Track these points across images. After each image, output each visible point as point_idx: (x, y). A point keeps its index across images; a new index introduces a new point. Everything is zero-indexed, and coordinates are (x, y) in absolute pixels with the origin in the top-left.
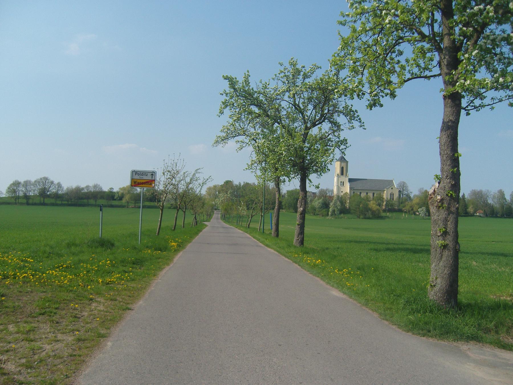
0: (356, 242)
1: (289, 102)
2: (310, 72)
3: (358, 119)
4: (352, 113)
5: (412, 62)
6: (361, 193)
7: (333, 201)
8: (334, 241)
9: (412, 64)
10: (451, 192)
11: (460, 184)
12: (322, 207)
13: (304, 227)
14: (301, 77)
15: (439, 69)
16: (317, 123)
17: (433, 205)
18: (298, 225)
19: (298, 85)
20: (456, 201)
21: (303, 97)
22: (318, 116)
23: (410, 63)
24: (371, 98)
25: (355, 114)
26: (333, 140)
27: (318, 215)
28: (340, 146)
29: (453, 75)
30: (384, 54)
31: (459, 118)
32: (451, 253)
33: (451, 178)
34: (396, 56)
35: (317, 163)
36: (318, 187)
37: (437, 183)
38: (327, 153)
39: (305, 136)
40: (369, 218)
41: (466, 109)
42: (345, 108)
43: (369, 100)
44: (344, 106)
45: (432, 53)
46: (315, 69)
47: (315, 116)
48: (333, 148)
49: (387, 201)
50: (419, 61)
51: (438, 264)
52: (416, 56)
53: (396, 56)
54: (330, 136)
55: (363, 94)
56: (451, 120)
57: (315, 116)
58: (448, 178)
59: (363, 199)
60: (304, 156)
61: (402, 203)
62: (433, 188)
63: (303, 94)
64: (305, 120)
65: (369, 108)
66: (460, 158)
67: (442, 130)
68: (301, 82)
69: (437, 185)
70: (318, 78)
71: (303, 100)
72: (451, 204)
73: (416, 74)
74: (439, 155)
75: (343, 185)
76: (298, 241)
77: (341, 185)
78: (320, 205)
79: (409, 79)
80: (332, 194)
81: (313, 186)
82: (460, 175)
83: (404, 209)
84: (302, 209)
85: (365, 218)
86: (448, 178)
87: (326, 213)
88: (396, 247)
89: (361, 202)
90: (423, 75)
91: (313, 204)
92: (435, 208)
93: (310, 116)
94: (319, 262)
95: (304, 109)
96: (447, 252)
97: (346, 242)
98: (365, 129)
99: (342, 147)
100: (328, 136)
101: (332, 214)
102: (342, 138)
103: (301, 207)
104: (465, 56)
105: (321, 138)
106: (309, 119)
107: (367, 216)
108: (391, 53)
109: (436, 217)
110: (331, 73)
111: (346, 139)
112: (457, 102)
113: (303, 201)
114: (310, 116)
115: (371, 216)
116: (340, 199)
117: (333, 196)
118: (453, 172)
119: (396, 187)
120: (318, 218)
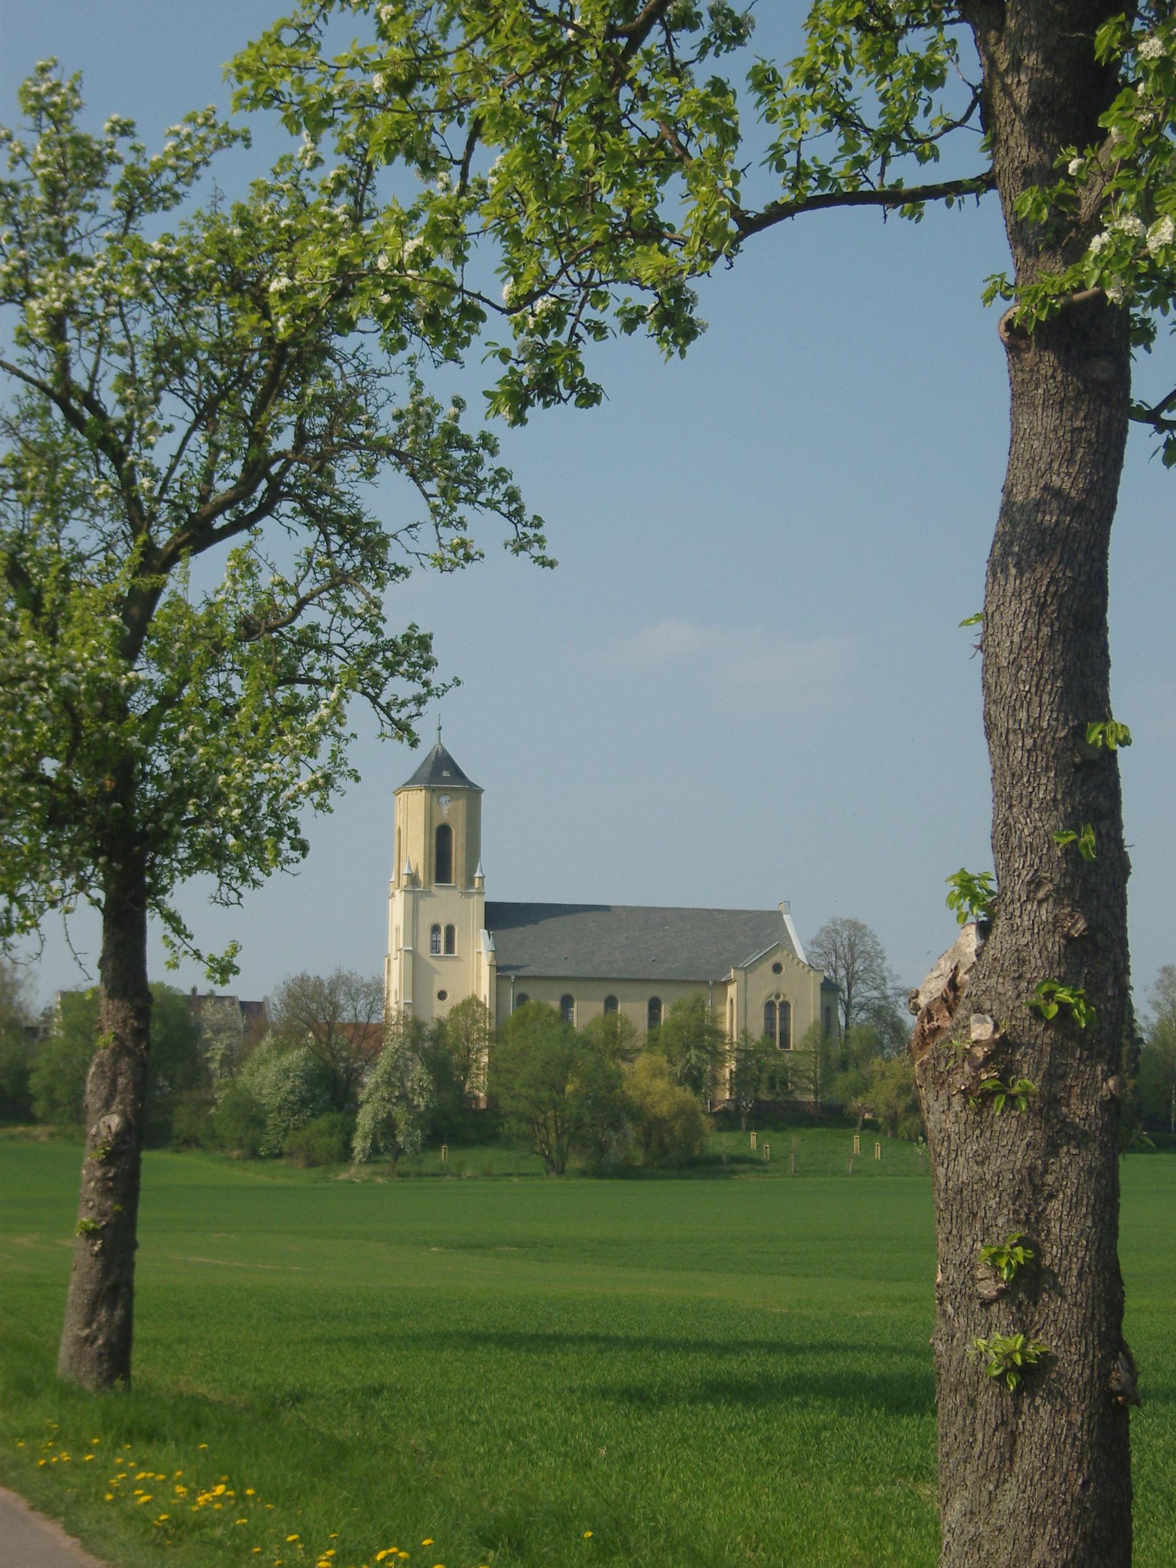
0: (510, 1341)
1: (20, 374)
2: (174, 169)
3: (497, 496)
4: (458, 454)
5: (792, 87)
6: (567, 1002)
7: (384, 1061)
8: (357, 1342)
9: (796, 107)
10: (1064, 995)
11: (1129, 936)
12: (303, 1102)
13: (131, 1246)
14: (107, 200)
15: (979, 139)
16: (219, 522)
17: (940, 1081)
18: (91, 1234)
19: (87, 253)
20: (1100, 1054)
21: (119, 340)
22: (225, 477)
23: (779, 96)
24: (522, 337)
25: (477, 462)
26: (336, 638)
27: (280, 1155)
28: (377, 682)
29: (1070, 179)
30: (612, 32)
31: (1116, 482)
32: (1077, 1418)
33: (1060, 894)
34: (703, 52)
35: (219, 797)
36: (224, 969)
37: (972, 930)
38: (293, 731)
39: (135, 611)
40: (626, 1172)
41: (1165, 415)
42: (410, 418)
43: (504, 356)
44: (406, 404)
45: (933, 31)
46: (209, 147)
47: (208, 475)
48: (333, 695)
49: (746, 1055)
50: (849, 86)
51: (985, 1498)
52: (821, 45)
53: (703, 52)
54: (311, 615)
55: (470, 313)
56: (1058, 493)
57: (208, 475)
58: (1041, 894)
59: (585, 1042)
60: (128, 749)
61: (844, 1066)
62: (946, 966)
63: (122, 316)
64: (134, 502)
65: (505, 412)
66: (1122, 754)
67: (996, 567)
68: (109, 232)
69: (970, 940)
70: (226, 209)
71: (123, 363)
72: (1063, 1077)
73: (824, 176)
74: (985, 741)
75: (450, 948)
76: (91, 1351)
77: (435, 948)
78: (289, 1085)
79: (777, 213)
80: (371, 1012)
81: (199, 957)
82: (1123, 868)
83: (857, 1103)
84: (115, 1121)
85: (599, 1172)
86: (1041, 894)
87: (335, 1141)
88: (781, 1367)
89: (567, 1064)
90: (876, 180)
91: (244, 1080)
92: (957, 1101)
93: (171, 469)
94: (219, 1498)
95: (128, 426)
96: (1045, 1411)
97: (442, 1340)
98: (552, 564)
99: (398, 687)
100: (297, 610)
101: (375, 1147)
102: (393, 630)
103: (107, 1105)
104: (1142, 47)
105: (248, 628)
106: (164, 489)
107: (614, 1155)
108: (668, 29)
109: (963, 1170)
110: (316, 177)
111: (421, 632)
112: (1102, 370)
113: (124, 1063)
114: (171, 469)
115: (639, 1157)
116: (427, 1045)
117: (382, 1028)
118: (1072, 851)
119: (801, 955)
120: (279, 1181)
